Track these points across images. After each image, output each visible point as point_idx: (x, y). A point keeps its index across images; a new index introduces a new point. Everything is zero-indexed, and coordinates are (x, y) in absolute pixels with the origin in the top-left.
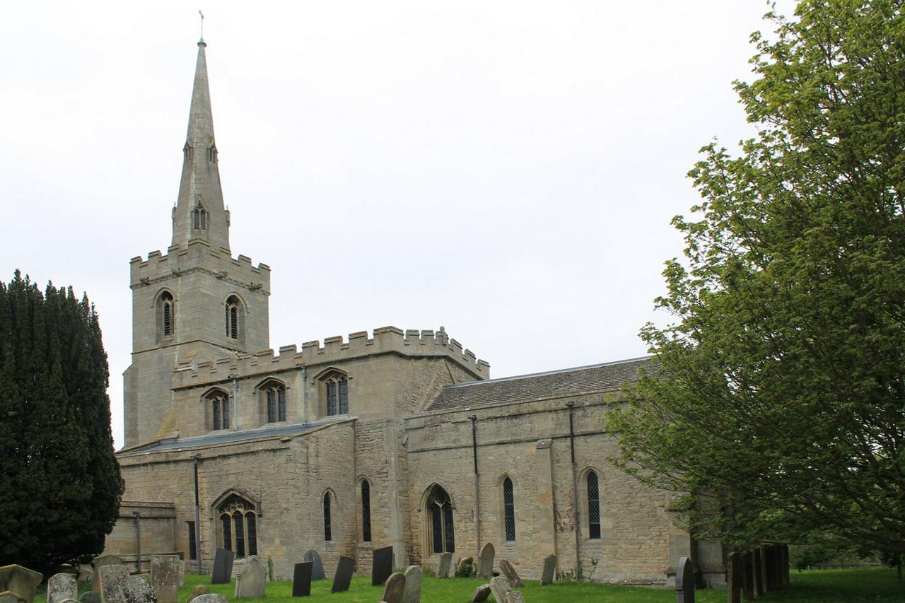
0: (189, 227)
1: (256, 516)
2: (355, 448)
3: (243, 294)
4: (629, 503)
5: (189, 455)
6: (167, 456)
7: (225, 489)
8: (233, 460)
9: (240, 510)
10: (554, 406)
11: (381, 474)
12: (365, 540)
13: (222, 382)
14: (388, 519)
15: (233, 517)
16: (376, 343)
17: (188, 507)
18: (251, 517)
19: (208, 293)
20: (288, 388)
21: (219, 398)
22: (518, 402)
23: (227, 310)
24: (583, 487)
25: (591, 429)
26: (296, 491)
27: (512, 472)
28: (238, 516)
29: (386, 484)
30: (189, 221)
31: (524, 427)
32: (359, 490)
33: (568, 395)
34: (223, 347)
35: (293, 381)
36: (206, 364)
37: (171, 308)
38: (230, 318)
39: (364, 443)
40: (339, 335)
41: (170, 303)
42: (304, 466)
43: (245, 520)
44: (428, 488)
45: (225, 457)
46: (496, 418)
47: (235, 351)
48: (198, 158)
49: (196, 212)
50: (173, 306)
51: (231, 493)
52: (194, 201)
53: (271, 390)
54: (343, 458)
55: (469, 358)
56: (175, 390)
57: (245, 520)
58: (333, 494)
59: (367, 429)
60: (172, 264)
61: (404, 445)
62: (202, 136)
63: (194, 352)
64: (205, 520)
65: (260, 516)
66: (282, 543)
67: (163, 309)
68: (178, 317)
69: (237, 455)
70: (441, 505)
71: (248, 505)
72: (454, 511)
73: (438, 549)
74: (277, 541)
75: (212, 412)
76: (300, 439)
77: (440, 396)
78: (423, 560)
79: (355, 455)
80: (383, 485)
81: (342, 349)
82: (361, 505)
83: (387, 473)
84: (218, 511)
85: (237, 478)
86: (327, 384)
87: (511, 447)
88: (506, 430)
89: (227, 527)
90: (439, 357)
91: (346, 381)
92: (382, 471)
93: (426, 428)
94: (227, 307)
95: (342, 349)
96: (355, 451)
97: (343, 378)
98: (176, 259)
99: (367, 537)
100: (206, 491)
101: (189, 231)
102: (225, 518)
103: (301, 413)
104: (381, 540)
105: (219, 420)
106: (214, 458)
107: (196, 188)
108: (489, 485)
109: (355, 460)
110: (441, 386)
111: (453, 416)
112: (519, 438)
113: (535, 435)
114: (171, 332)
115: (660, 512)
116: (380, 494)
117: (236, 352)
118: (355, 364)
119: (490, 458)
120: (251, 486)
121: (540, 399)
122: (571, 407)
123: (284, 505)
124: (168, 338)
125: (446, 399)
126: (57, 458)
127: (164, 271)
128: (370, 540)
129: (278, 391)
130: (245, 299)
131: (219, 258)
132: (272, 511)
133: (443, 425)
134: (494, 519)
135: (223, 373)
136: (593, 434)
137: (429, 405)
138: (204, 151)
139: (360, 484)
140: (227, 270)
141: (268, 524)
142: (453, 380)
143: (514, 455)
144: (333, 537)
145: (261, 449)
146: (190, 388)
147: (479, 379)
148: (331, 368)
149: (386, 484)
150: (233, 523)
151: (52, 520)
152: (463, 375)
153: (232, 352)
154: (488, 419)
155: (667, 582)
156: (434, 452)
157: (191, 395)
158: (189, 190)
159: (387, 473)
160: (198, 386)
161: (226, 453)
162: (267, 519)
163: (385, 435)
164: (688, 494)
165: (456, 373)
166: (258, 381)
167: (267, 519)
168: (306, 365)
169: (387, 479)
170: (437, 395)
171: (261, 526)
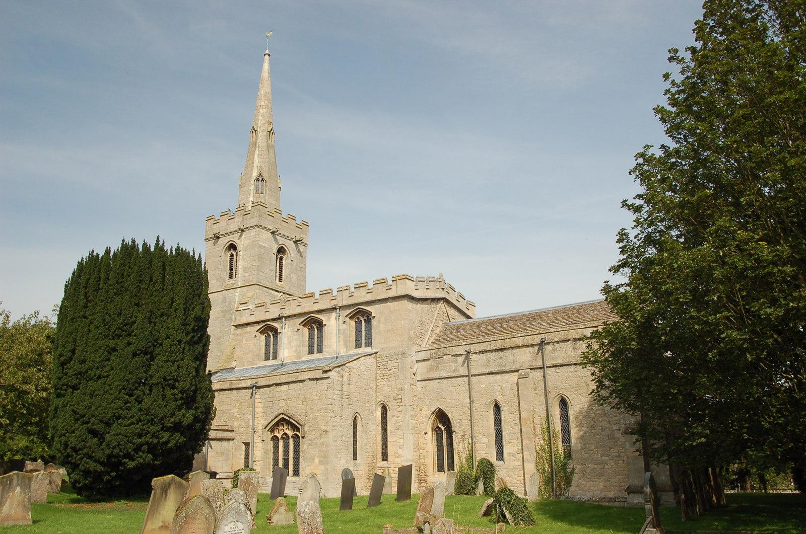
0: (252, 192)
1: (300, 438)
2: (376, 377)
3: (290, 246)
4: (592, 427)
5: (249, 383)
6: (231, 384)
7: (276, 413)
8: (284, 387)
9: (287, 431)
10: (530, 342)
11: (396, 400)
12: (383, 460)
13: (274, 320)
14: (402, 440)
15: (292, 437)
16: (394, 288)
17: (245, 429)
18: (296, 437)
19: (264, 245)
20: (325, 325)
21: (270, 333)
22: (503, 338)
23: (277, 258)
24: (556, 412)
25: (560, 361)
26: (333, 415)
27: (500, 399)
28: (286, 437)
29: (401, 408)
30: (252, 187)
31: (510, 359)
32: (379, 414)
33: (541, 332)
34: (273, 290)
35: (329, 319)
36: (262, 305)
37: (235, 257)
38: (278, 265)
39: (384, 372)
40: (384, 277)
41: (234, 254)
42: (340, 393)
43: (291, 441)
44: (433, 413)
45: (277, 385)
46: (486, 351)
47: (281, 292)
48: (261, 138)
49: (258, 180)
50: (237, 255)
51: (281, 416)
52: (256, 171)
53: (312, 326)
54: (367, 385)
55: (461, 299)
56: (235, 326)
57: (291, 441)
58: (360, 417)
59: (386, 360)
60: (238, 222)
61: (414, 374)
62: (264, 122)
63: (250, 294)
64: (258, 441)
65: (303, 437)
66: (321, 463)
67: (229, 258)
68: (241, 264)
69: (288, 383)
70: (443, 428)
71: (295, 427)
72: (454, 433)
73: (441, 469)
74: (317, 460)
75: (264, 345)
76: (337, 369)
77: (440, 332)
78: (429, 479)
79: (376, 383)
80: (398, 409)
81: (367, 293)
82: (380, 428)
83: (401, 399)
84: (269, 433)
85: (287, 404)
86: (356, 321)
87: (498, 376)
88: (494, 361)
89: (276, 447)
90: (439, 299)
91: (371, 319)
92: (397, 398)
93: (431, 360)
94: (277, 256)
95: (367, 293)
96: (376, 380)
97: (368, 317)
98: (241, 218)
99: (385, 457)
100: (261, 415)
101: (252, 195)
102: (275, 439)
103: (334, 346)
104: (397, 460)
105: (271, 352)
106: (269, 386)
107: (259, 162)
108: (482, 410)
109: (376, 388)
110: (441, 323)
111: (452, 349)
112: (504, 368)
113: (517, 366)
114: (234, 276)
115: (618, 434)
116: (395, 418)
117: (282, 293)
118: (377, 306)
119: (482, 386)
120: (297, 412)
121: (519, 335)
122: (542, 344)
123: (324, 428)
124: (231, 281)
125: (449, 335)
126: (28, 404)
127: (231, 227)
128: (387, 460)
129: (273, 335)
130: (290, 249)
131: (273, 217)
132: (314, 433)
133: (445, 357)
134: (485, 440)
135: (274, 312)
136: (562, 366)
137: (432, 339)
138: (265, 133)
139: (380, 409)
140: (278, 227)
141: (310, 445)
142: (449, 317)
143: (501, 384)
144: (358, 457)
145: (307, 378)
146: (248, 324)
147: (468, 317)
148: (311, 316)
149: (401, 408)
150: (281, 443)
151: (164, 440)
152: (457, 314)
153: (278, 294)
154: (480, 352)
155: (628, 500)
156: (438, 381)
157: (248, 330)
158: (253, 163)
159: (401, 399)
160: (254, 323)
161: (279, 382)
162: (309, 440)
163: (400, 365)
164: (640, 418)
165: (452, 312)
166: (259, 327)
167: (309, 440)
168: (340, 305)
169: (401, 404)
170: (438, 331)
171: (304, 446)
